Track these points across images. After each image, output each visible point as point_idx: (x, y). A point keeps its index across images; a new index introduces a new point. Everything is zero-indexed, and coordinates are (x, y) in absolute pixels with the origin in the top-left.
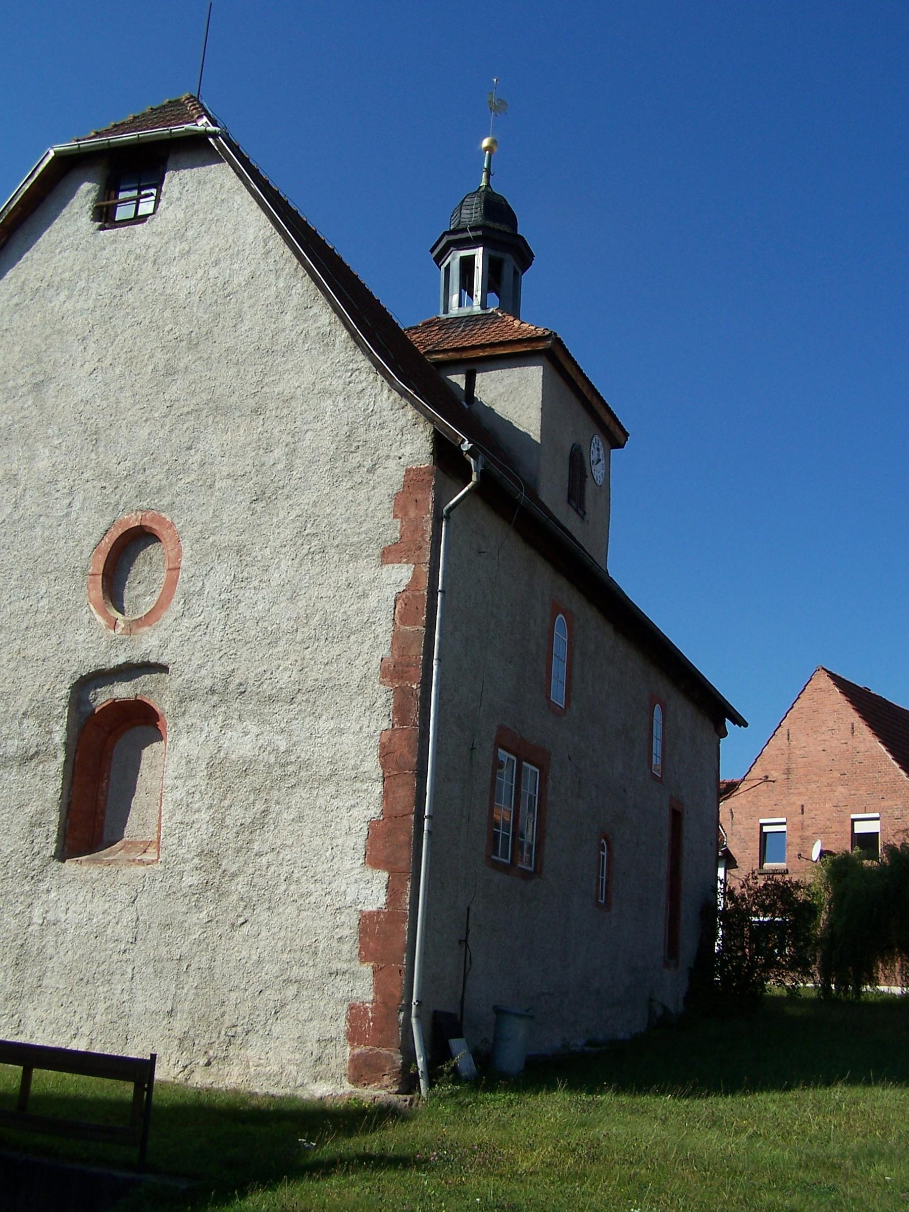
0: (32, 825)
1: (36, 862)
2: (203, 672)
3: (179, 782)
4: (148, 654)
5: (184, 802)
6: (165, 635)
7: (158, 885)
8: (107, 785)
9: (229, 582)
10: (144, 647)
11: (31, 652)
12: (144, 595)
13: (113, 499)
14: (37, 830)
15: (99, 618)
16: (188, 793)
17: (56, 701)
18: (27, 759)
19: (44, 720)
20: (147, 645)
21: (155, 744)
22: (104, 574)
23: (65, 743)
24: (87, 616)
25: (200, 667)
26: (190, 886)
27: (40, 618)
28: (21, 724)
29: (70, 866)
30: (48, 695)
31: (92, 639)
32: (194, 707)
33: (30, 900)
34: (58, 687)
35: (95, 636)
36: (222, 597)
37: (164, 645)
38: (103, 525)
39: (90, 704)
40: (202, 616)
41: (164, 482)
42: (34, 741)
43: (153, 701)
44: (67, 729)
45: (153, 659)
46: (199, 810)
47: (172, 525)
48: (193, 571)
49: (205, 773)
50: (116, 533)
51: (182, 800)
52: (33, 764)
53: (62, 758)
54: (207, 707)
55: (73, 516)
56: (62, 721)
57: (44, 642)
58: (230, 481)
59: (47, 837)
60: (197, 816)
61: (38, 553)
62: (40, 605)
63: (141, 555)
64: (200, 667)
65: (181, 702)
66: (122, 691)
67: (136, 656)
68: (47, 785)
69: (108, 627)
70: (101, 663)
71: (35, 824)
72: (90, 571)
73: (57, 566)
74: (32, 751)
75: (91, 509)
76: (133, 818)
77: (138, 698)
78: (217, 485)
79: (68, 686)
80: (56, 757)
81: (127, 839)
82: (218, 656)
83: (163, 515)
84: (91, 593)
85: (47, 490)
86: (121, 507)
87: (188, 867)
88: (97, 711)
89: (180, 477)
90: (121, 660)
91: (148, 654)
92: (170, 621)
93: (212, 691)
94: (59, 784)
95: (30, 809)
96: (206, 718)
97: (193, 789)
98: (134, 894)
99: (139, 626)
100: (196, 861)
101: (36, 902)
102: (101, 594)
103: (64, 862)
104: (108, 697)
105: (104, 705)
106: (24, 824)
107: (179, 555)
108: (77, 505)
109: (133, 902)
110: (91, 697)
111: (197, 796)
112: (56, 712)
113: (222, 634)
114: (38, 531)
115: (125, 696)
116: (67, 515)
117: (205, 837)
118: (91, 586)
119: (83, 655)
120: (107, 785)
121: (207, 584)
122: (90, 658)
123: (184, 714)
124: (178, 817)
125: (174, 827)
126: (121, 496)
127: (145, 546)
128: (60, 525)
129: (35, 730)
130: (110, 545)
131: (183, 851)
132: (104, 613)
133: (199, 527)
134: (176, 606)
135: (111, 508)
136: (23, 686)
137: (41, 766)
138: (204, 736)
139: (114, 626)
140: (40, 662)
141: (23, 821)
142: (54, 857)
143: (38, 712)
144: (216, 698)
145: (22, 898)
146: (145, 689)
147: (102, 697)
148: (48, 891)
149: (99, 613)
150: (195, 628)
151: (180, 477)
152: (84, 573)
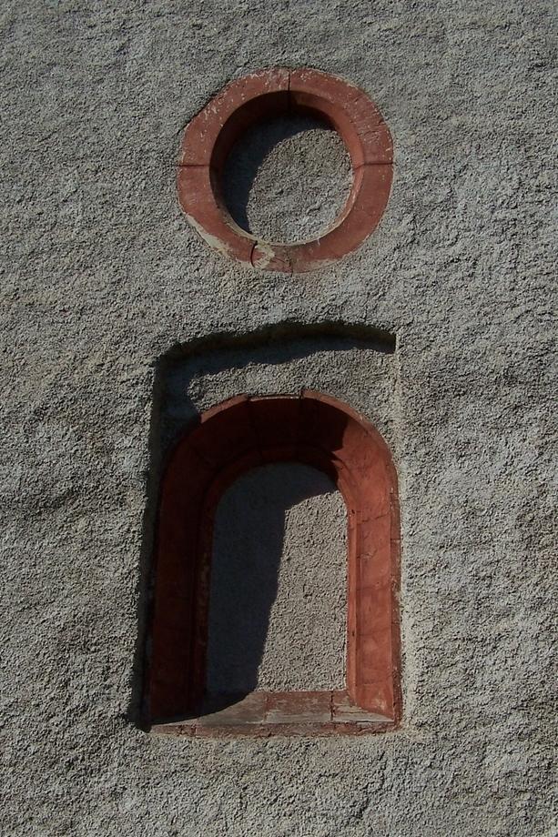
0: (63, 647)
1: (80, 728)
2: (481, 343)
3: (452, 555)
4: (342, 307)
5: (470, 597)
6: (379, 274)
7: (420, 775)
8: (208, 575)
9: (510, 192)
10: (328, 294)
11: (47, 295)
12: (297, 213)
13: (223, 45)
14: (77, 659)
15: (212, 240)
16: (476, 578)
17: (122, 389)
18: (40, 505)
19: (92, 423)
20: (339, 290)
21: (316, 499)
22: (214, 168)
23: (146, 474)
24: (183, 237)
25: (472, 333)
26: (509, 775)
27: (61, 236)
28: (30, 432)
29: (162, 737)
30: (98, 376)
31: (195, 278)
32: (467, 408)
33: (66, 816)
34: (122, 360)
35: (209, 268)
36: (500, 215)
37: (378, 291)
38: (204, 84)
39: (193, 408)
40: (459, 244)
41: (334, 26)
42: (65, 469)
43: (349, 401)
44: (150, 445)
45: (351, 316)
46: (507, 613)
47: (360, 94)
48: (423, 168)
49: (517, 535)
50: (235, 101)
51: (462, 591)
52: (60, 516)
53: (137, 504)
54: (495, 411)
55: (130, 69)
56: (137, 428)
57: (79, 280)
58: (479, 34)
59: (106, 673)
60: (504, 624)
61: (51, 125)
62: (62, 213)
63: (280, 146)
64: (472, 333)
65: (435, 396)
66: (267, 380)
67: (312, 309)
68: (103, 561)
69: (234, 256)
70: (224, 321)
71: (75, 640)
72: (181, 159)
73: (96, 147)
74: (61, 488)
75: (173, 58)
76: (277, 645)
77: (308, 395)
78: (451, 39)
79: (149, 360)
80: (122, 502)
81: (267, 689)
82: (511, 315)
83: (339, 77)
84: (187, 197)
85: (65, 24)
86: (241, 60)
87: (498, 732)
88: (205, 417)
89: (369, 19)
90: (276, 315)
91: (342, 307)
92: (385, 250)
93: (510, 379)
94: (132, 559)
95: (58, 613)
96: (500, 430)
97: (489, 570)
98: (361, 798)
99: (310, 258)
100: (517, 719)
101: (83, 821)
102: (211, 198)
103: (147, 731)
104: (235, 391)
105: (224, 407)
106: (42, 645)
107: (386, 140)
108: (139, 50)
109: (360, 815)
110: (193, 389)
111: (501, 583)
112: (121, 411)
113: (510, 277)
114: (49, 88)
115: (276, 389)
116: (117, 65)
117: (533, 668)
118: (184, 184)
119: (178, 304)
120: (208, 575)
121: (461, 193)
122: (197, 310)
123: (444, 420)
124: (458, 627)
125: (449, 647)
126: (239, 42)
127: (288, 133)
128: (101, 81)
129: (67, 446)
130: (222, 119)
131: (479, 699)
132: (222, 232)
133: (424, 101)
134: (395, 225)
135: (218, 59)
136: (32, 359)
137: (82, 523)
138: (499, 465)
139: (251, 253)
140: (70, 316)
141: (37, 639)
142: (127, 718)
143: (82, 411)
144: (517, 393)
145: (45, 811)
146: (322, 378)
147: (218, 391)
148: (115, 795)
149: (209, 231)
150: (447, 264)
151: (369, 19)
152: (165, 160)
